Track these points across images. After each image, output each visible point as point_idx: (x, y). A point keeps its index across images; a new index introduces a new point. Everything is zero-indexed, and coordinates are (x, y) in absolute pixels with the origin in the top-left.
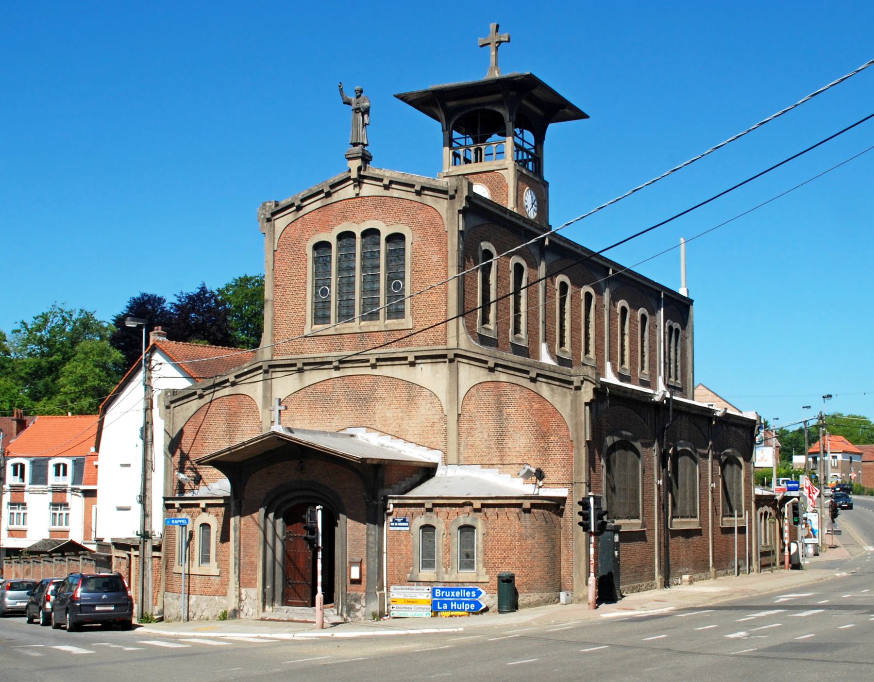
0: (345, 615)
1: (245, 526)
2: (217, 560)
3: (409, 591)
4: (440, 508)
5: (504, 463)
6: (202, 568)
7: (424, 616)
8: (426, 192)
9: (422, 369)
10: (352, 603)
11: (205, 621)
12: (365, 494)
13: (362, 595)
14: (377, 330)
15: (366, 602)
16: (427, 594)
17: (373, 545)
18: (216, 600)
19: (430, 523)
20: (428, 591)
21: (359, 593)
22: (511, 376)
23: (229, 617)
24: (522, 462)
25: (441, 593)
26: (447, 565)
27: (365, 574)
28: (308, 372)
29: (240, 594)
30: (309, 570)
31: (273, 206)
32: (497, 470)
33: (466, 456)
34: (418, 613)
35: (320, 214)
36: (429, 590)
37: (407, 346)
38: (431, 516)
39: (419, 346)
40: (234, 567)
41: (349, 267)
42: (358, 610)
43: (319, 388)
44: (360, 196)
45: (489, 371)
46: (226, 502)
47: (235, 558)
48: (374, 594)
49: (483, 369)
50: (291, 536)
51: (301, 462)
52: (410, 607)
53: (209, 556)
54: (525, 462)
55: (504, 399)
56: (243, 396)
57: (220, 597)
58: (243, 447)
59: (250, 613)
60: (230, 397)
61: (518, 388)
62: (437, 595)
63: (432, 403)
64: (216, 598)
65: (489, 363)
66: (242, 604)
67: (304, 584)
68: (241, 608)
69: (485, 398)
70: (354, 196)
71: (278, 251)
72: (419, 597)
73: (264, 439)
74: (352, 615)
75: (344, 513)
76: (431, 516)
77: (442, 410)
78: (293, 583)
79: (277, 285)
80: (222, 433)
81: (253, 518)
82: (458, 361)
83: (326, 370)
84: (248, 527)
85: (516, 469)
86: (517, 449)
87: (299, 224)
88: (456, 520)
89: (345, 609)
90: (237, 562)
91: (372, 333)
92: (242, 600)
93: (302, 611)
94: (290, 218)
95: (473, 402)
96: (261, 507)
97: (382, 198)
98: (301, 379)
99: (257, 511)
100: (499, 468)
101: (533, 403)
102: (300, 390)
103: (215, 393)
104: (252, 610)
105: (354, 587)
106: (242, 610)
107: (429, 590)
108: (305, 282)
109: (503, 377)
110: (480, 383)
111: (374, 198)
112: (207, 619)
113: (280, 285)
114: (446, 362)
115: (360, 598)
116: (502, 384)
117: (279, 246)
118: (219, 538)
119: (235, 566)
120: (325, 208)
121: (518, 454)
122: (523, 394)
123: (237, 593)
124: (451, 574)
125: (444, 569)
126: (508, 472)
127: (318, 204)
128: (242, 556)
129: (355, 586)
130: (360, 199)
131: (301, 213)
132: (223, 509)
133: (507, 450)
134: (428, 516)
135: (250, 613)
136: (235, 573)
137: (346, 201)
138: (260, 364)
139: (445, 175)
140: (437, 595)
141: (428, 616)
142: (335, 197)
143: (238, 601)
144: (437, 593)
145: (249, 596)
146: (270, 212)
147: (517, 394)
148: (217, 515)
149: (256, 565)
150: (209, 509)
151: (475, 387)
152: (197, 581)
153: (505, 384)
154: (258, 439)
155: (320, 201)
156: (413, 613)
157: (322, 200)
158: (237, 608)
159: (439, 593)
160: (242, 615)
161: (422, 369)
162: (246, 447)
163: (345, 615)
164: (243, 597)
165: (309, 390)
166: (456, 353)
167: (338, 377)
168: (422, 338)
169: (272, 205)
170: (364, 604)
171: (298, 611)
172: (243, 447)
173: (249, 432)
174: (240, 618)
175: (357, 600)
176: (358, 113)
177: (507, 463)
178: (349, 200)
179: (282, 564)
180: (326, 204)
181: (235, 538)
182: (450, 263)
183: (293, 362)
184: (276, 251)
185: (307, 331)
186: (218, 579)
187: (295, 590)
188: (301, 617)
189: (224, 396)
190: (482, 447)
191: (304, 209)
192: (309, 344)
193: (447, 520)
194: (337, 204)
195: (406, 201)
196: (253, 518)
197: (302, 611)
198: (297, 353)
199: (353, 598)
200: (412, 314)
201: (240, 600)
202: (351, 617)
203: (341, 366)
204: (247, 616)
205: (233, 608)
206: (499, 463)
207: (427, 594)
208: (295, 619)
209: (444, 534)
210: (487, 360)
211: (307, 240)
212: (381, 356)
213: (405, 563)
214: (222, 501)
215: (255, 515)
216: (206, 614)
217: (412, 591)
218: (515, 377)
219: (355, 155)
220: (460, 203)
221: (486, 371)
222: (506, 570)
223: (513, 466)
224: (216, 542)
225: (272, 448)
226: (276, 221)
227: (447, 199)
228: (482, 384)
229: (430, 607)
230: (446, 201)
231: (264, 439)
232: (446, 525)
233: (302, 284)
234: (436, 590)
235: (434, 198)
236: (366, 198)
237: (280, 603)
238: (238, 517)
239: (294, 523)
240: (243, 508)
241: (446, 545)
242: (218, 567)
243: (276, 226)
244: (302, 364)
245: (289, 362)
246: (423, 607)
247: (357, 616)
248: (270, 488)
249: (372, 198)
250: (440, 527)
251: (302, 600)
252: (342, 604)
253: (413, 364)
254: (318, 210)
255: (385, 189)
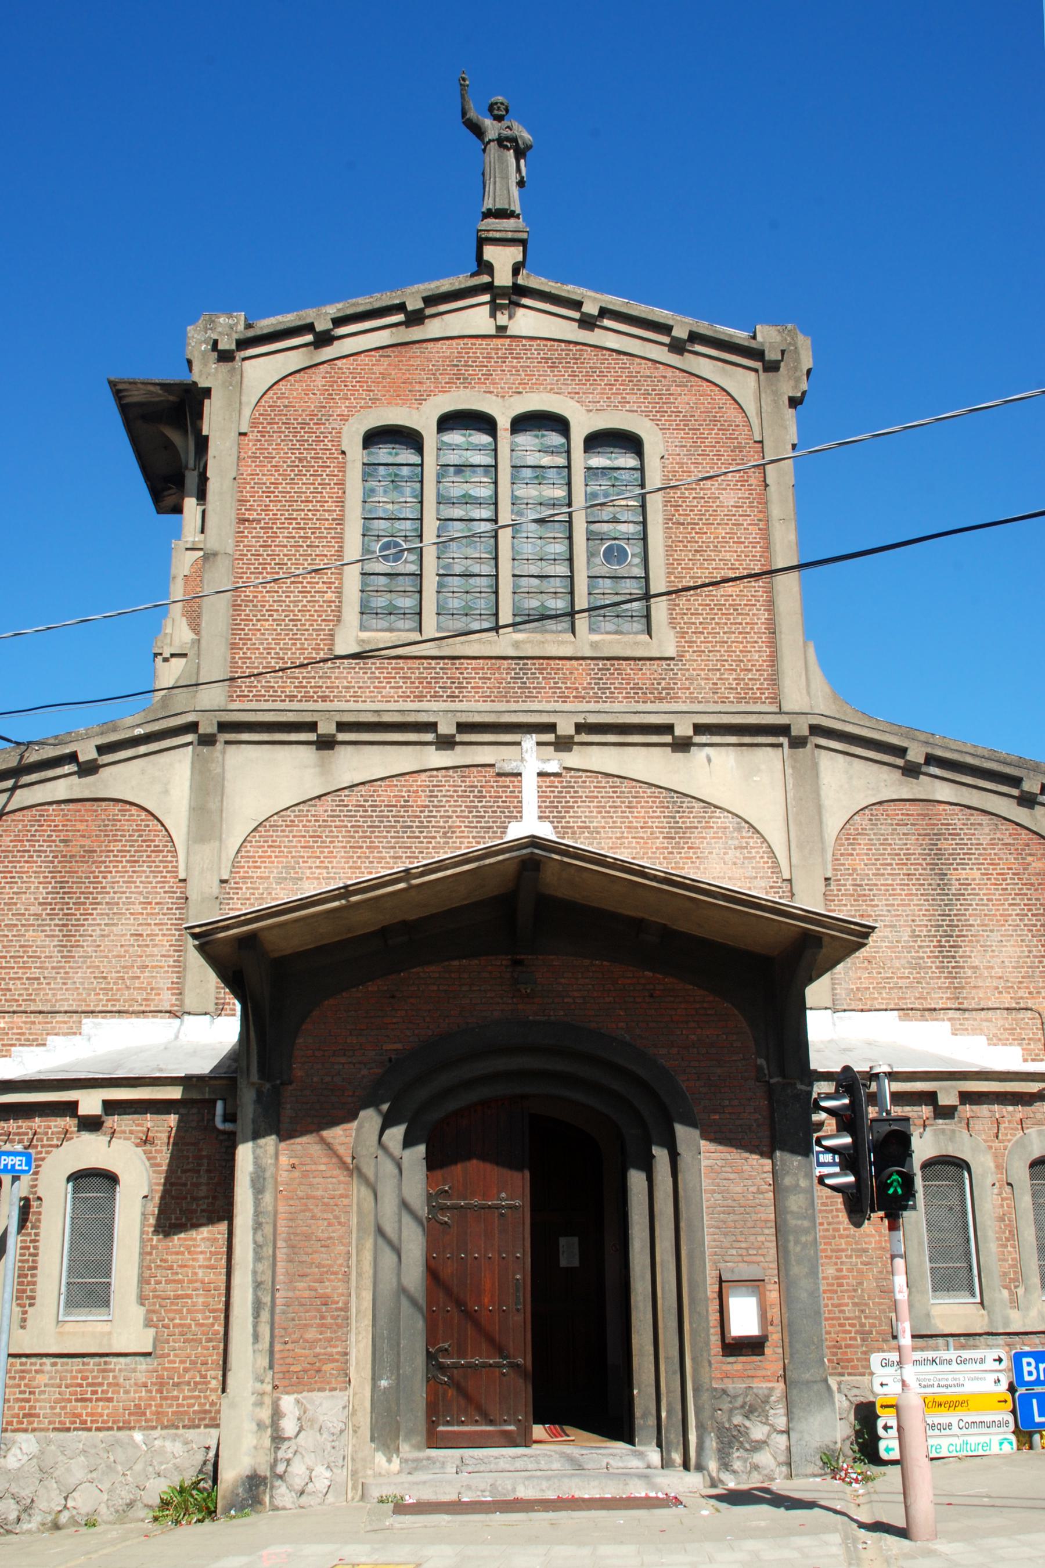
0: (713, 1465)
1: (297, 1174)
2: (142, 1299)
3: (934, 1368)
4: (974, 1107)
5: (965, 1006)
6: (68, 1327)
7: (995, 1449)
8: (698, 348)
9: (709, 760)
10: (738, 1420)
11: (84, 1530)
12: (761, 1062)
13: (772, 1389)
14: (569, 655)
15: (789, 1414)
16: (995, 1376)
17: (806, 1224)
18: (136, 1446)
19: (951, 1151)
20: (996, 1366)
21: (761, 1386)
22: (964, 788)
23: (227, 1511)
24: (1014, 1005)
25: (1037, 1368)
26: (1012, 1280)
27: (777, 1320)
28: (350, 748)
29: (277, 1414)
30: (519, 1318)
31: (241, 327)
32: (947, 1025)
33: (854, 987)
34: (973, 1440)
35: (385, 362)
36: (1000, 1360)
37: (661, 699)
38: (953, 1131)
39: (693, 700)
40: (250, 1319)
41: (470, 496)
42: (758, 1446)
43: (385, 794)
44: (509, 333)
45: (903, 774)
46: (188, 1096)
47: (258, 1285)
48: (821, 1386)
49: (885, 768)
50: (443, 1209)
51: (516, 963)
52: (944, 1420)
53: (109, 1284)
54: (1022, 1005)
55: (947, 845)
56: (120, 806)
57: (156, 1433)
58: (402, 885)
59: (321, 1482)
60: (71, 806)
61: (985, 819)
62: (1027, 1378)
63: (742, 848)
64: (138, 1436)
65: (909, 752)
66: (281, 1454)
67: (499, 1366)
68: (280, 1468)
69: (897, 842)
70: (493, 331)
71: (251, 436)
72: (971, 1387)
73: (487, 861)
74: (737, 1465)
75: (691, 1123)
76: (953, 1131)
77: (776, 864)
78: (456, 1366)
79: (248, 520)
80: (38, 909)
81: (328, 1146)
82: (817, 746)
83: (410, 748)
84: (305, 1174)
85: (1000, 1023)
86: (998, 971)
87: (318, 379)
88: (1020, 1143)
89: (712, 1443)
90: (267, 1299)
91: (552, 662)
92: (285, 1439)
93: (519, 1464)
94: (295, 360)
95: (859, 850)
96: (365, 1106)
97: (571, 347)
98: (324, 768)
99: (352, 1116)
100: (949, 1019)
101: (1030, 859)
102: (319, 797)
103: (18, 792)
104: (328, 1474)
105: (738, 1367)
106: (281, 1477)
107: (1000, 1360)
108: (340, 521)
109: (944, 792)
110: (880, 803)
111: (549, 343)
112: (91, 1524)
113: (259, 521)
114: (781, 745)
115: (766, 1401)
116: (942, 807)
117: (254, 424)
118: (152, 1221)
119: (256, 1315)
120: (403, 349)
121: (1001, 984)
122: (998, 836)
123: (265, 1414)
124: (1027, 1309)
125: (1005, 1293)
126: (977, 1031)
127: (383, 338)
128: (280, 1278)
129: (738, 1364)
130: (508, 341)
131: (328, 352)
132: (173, 1119)
133: (969, 972)
134: (943, 1131)
135: (321, 1482)
136: (256, 1337)
137: (466, 341)
138: (191, 718)
139: (188, 546)
140: (1027, 1378)
141: (1007, 1449)
142: (433, 328)
143: (267, 1442)
144: (1026, 1369)
145: (312, 1421)
146: (235, 336)
147: (984, 832)
148: (146, 1141)
149: (346, 1309)
150: (112, 1121)
151: (867, 811)
152: (42, 1379)
153: (947, 807)
154: (465, 859)
155: (387, 332)
156: (958, 1441)
157: (394, 330)
158: (264, 1471)
159: (1032, 1368)
160: (283, 1495)
161: (709, 760)
162: (411, 887)
163: (713, 1465)
164: (289, 1426)
165: (352, 799)
166: (815, 722)
167: (446, 768)
168: (703, 683)
169: (236, 324)
170: (781, 1422)
171: (502, 1464)
172: (402, 885)
173: (138, 908)
174: (276, 1508)
175: (754, 1409)
176: (508, 149)
177: (974, 1006)
178: (473, 341)
179: (422, 1301)
180: (408, 340)
181: (257, 1213)
182: (776, 511)
183: (308, 718)
184: (245, 434)
185: (347, 642)
186: (143, 1364)
187: (461, 1390)
188: (544, 1484)
189: (51, 803)
190: (897, 963)
191: (336, 343)
192: (348, 675)
193: (996, 1144)
194: (439, 344)
195: (638, 360)
196: (323, 1141)
197: (519, 1464)
198: (308, 698)
199: (739, 1402)
200: (672, 623)
201: (278, 1439)
202: (734, 1472)
203: (459, 738)
204: (304, 1500)
205: (248, 1472)
206: (949, 1006)
207: (995, 1376)
208: (525, 1492)
209: (994, 1185)
210: (905, 745)
211: (344, 418)
212: (592, 719)
213: (877, 1279)
214: (175, 1093)
215: (337, 1135)
216: (82, 1502)
217: (946, 1368)
218: (975, 791)
219: (510, 235)
220: (792, 383)
221: (897, 774)
222: (22, 1331)
223: (990, 1014)
224: (142, 1233)
225: (412, 916)
226: (247, 363)
227: (756, 371)
228: (885, 806)
229: (1010, 1418)
230: (753, 374)
231: (487, 861)
232: (996, 1156)
233: (327, 524)
234: (1025, 1360)
235: (720, 364)
236: (524, 342)
237: (421, 1438)
238: (269, 1142)
239: (454, 1162)
240: (287, 1111)
241: (1001, 1219)
242: (148, 1323)
243: (245, 375)
244: (334, 726)
245: (291, 717)
246: (988, 1418)
247: (756, 1467)
248: (399, 1046)
249: (542, 343)
250: (983, 1164)
251: (491, 1422)
252: (700, 1427)
253: (683, 745)
254: (381, 352)
255: (579, 327)
